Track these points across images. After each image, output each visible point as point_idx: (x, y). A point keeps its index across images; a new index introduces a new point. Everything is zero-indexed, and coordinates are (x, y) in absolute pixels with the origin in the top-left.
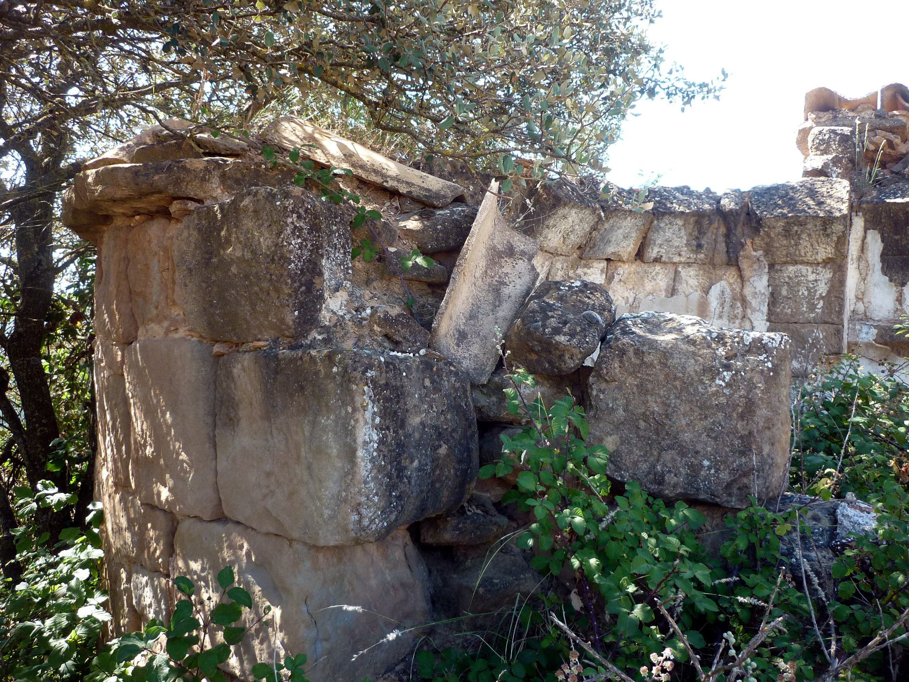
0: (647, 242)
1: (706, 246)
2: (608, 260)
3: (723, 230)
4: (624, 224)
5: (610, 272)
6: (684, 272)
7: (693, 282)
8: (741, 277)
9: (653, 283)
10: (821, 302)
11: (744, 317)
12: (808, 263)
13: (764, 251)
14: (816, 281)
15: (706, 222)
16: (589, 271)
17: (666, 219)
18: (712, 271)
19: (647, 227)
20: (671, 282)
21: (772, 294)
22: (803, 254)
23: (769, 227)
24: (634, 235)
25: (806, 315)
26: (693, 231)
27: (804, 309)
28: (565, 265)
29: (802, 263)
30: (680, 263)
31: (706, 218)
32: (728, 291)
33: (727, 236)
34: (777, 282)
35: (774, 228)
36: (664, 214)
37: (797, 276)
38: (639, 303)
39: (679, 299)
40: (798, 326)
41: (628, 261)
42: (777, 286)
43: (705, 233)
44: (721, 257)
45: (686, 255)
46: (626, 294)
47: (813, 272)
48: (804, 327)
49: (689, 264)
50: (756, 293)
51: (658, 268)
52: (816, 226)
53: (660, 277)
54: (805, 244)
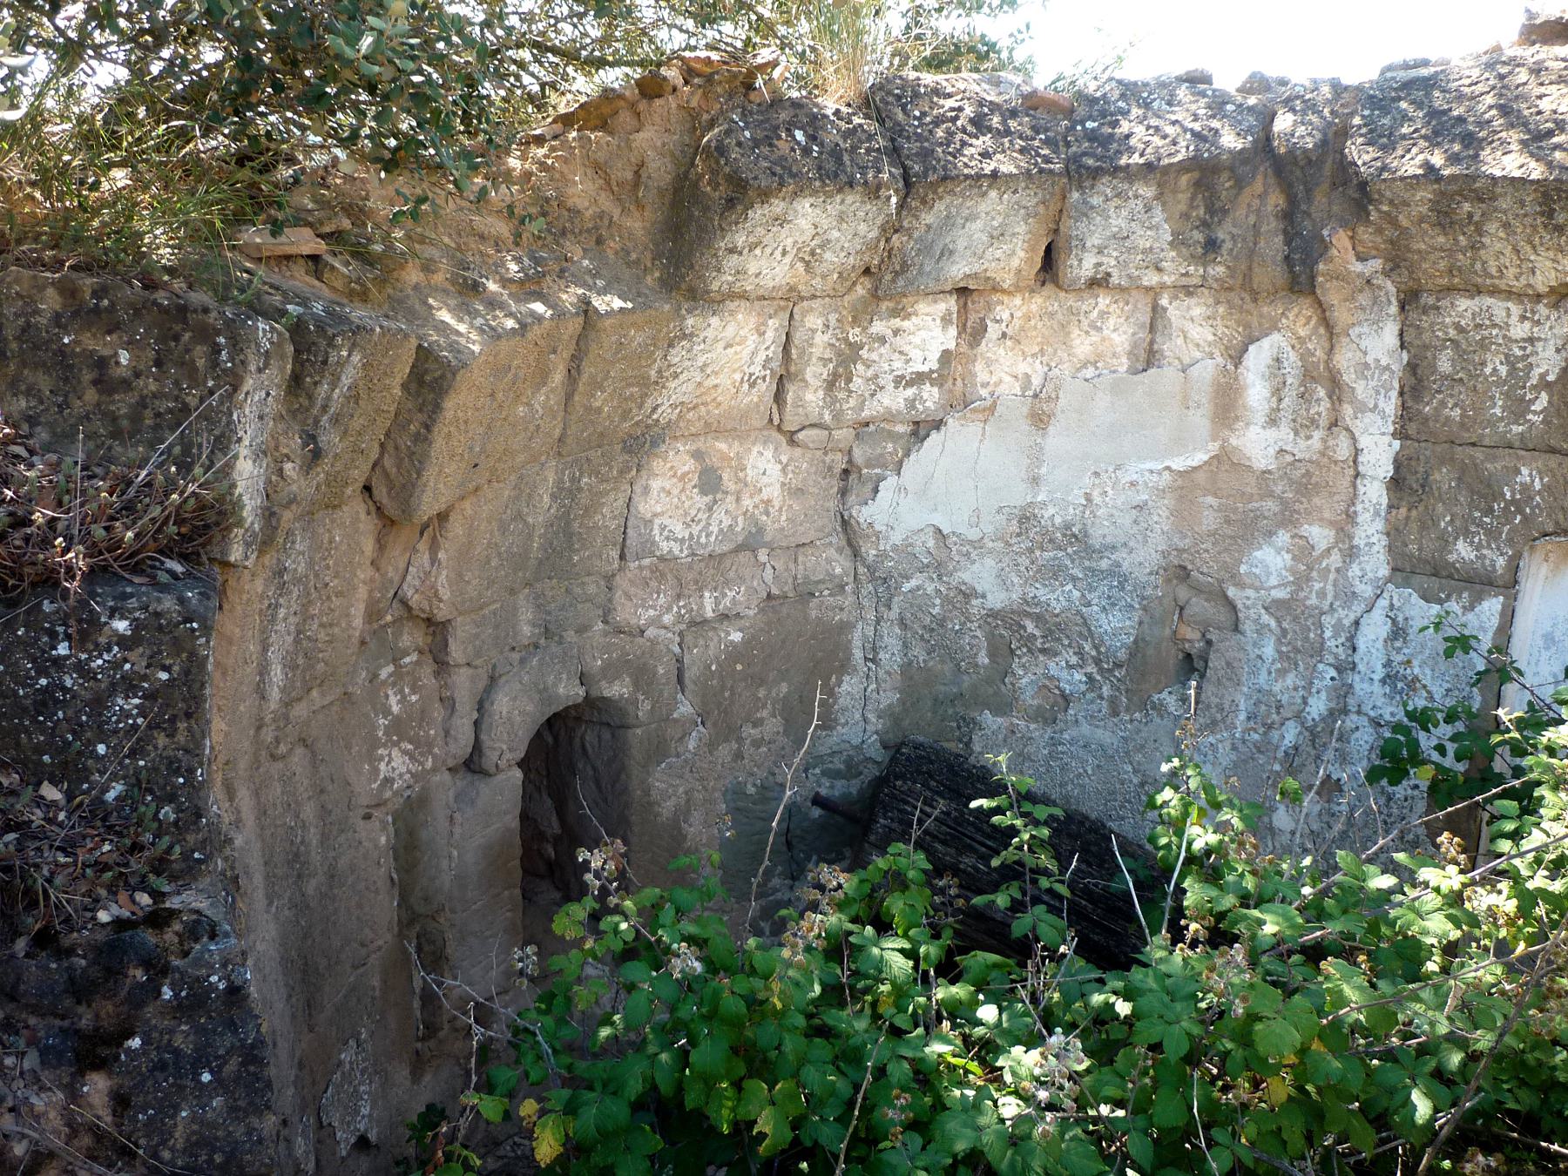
0: (1061, 243)
1: (1228, 245)
2: (963, 292)
3: (1276, 200)
4: (983, 207)
5: (973, 318)
6: (1175, 310)
7: (1202, 333)
8: (1327, 323)
9: (1095, 337)
10: (1544, 396)
11: (1335, 424)
12: (1509, 294)
13: (1387, 260)
14: (1531, 340)
15: (1225, 183)
16: (906, 324)
17: (1105, 186)
18: (1249, 306)
19: (1054, 207)
20: (1143, 335)
21: (1412, 367)
22: (1494, 271)
23: (1391, 202)
24: (1021, 228)
25: (1501, 427)
26: (1191, 207)
27: (1498, 411)
28: (833, 318)
29: (1494, 292)
30: (1163, 286)
31: (1225, 175)
32: (1292, 359)
33: (1288, 216)
34: (1426, 337)
35: (1406, 204)
36: (1095, 174)
37: (1479, 326)
38: (1057, 389)
39: (1165, 377)
40: (1479, 454)
41: (1018, 288)
42: (1426, 347)
43: (1225, 212)
44: (1270, 273)
45: (1174, 267)
46: (1023, 368)
47: (1523, 318)
48: (1494, 458)
49: (1189, 291)
50: (1367, 366)
51: (1104, 301)
52: (1522, 204)
53: (1111, 322)
54: (1498, 246)
